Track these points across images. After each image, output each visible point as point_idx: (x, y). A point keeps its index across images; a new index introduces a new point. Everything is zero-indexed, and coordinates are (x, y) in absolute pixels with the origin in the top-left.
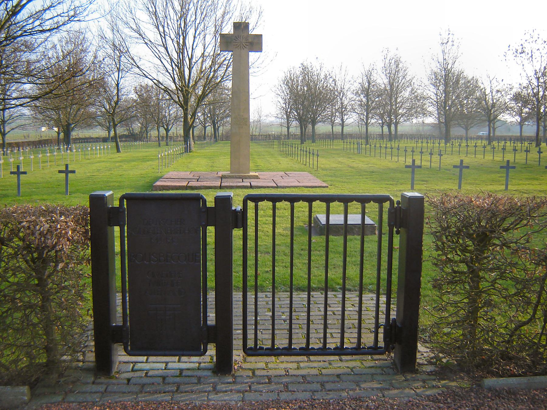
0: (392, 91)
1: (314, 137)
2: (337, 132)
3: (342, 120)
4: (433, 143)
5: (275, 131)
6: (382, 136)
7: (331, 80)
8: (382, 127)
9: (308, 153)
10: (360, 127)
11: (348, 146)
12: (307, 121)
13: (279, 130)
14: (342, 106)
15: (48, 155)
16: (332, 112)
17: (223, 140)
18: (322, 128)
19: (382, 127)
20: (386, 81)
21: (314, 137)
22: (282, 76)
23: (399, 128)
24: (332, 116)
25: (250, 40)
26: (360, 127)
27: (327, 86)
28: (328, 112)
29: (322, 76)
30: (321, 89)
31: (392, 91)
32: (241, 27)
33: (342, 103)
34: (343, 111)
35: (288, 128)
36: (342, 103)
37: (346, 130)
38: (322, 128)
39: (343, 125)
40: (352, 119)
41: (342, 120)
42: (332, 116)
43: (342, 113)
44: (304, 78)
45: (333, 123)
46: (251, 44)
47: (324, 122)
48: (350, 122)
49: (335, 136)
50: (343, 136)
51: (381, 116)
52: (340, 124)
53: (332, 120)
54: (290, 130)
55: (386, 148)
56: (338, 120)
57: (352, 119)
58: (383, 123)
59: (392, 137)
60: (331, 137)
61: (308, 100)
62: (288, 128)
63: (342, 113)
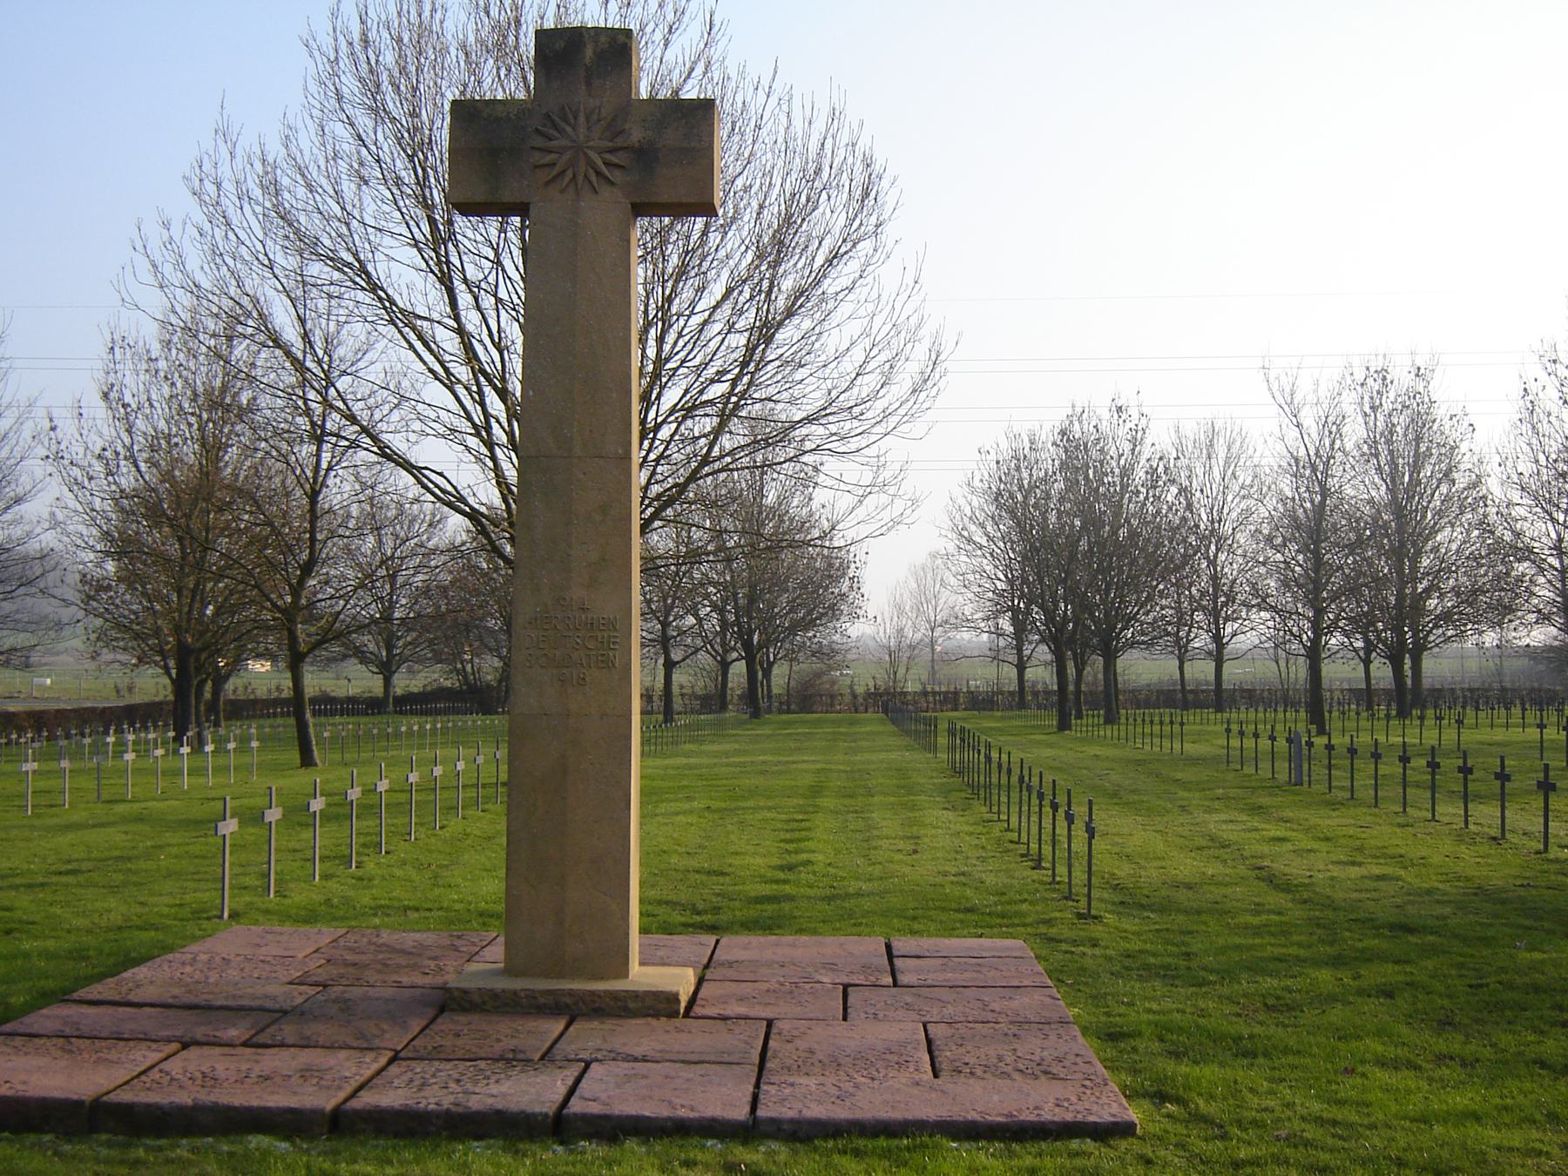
0: (1402, 527)
1: (1112, 701)
2: (1199, 683)
3: (1217, 638)
4: (1542, 726)
5: (981, 677)
6: (1366, 696)
7: (1174, 490)
8: (1367, 662)
9: (1005, 766)
10: (1282, 664)
11: (1147, 730)
12: (1085, 645)
13: (990, 672)
14: (1216, 587)
15: (30, 766)
16: (1178, 609)
17: (789, 712)
18: (1143, 667)
19: (1367, 662)
20: (1381, 493)
21: (1112, 701)
22: (984, 472)
23: (1427, 663)
24: (1180, 623)
25: (636, 135)
26: (1282, 664)
27: (1158, 512)
28: (1164, 608)
29: (1140, 475)
30: (1135, 522)
31: (1402, 527)
32: (584, 60)
33: (1215, 579)
34: (1219, 603)
35: (1021, 667)
36: (1215, 579)
37: (1234, 673)
38: (1143, 667)
39: (1218, 655)
40: (1251, 633)
41: (1217, 638)
42: (1180, 623)
43: (1214, 614)
44: (1071, 485)
45: (1182, 652)
46: (645, 156)
47: (1149, 645)
48: (1244, 647)
49: (1190, 697)
50: (1219, 698)
51: (1362, 624)
52: (1209, 653)
53: (1179, 639)
54: (1030, 674)
55: (1256, 736)
56: (1202, 640)
57: (1251, 633)
58: (1369, 647)
59: (1409, 698)
60: (1179, 698)
61: (1086, 555)
62: (1021, 667)
63: (1214, 614)
